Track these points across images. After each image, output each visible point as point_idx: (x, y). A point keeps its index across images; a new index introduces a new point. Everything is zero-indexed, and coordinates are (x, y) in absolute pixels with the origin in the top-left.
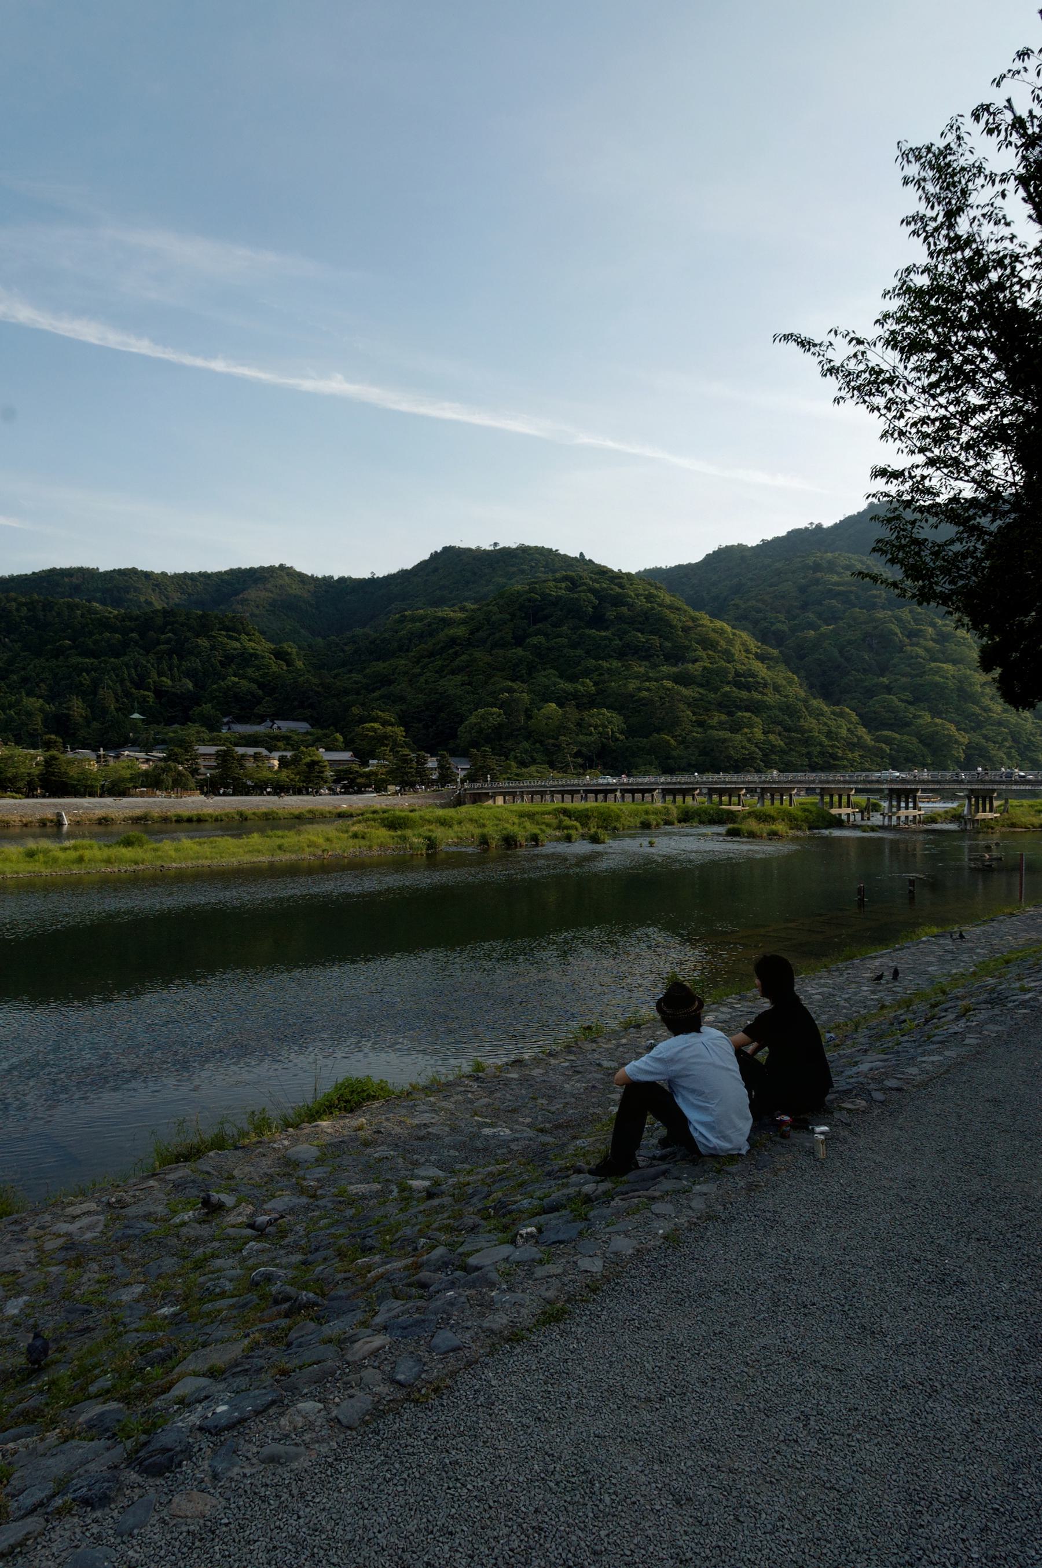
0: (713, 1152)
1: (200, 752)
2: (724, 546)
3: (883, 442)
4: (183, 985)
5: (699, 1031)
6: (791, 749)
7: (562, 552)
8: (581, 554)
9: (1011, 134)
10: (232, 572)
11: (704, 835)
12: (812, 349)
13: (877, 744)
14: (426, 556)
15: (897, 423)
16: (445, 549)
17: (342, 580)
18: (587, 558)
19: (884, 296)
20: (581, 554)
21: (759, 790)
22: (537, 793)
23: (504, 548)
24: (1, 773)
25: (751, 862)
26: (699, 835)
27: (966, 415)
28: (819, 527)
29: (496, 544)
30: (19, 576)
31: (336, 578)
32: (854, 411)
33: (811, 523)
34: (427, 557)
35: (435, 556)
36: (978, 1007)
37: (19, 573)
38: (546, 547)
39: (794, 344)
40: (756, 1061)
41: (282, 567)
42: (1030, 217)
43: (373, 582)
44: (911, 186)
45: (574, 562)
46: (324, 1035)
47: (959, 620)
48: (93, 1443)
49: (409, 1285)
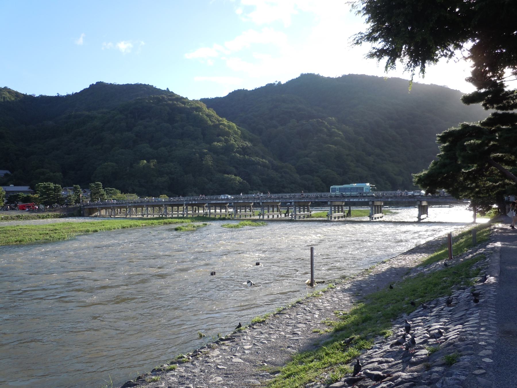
3: (358, 46)
4: (345, 317)
12: (356, 7)
14: (264, 85)
16: (97, 83)
18: (171, 90)
19: (58, 93)
20: (167, 88)
22: (175, 205)
24: (516, 74)
26: (121, 368)
30: (50, 96)
32: (426, 70)
33: (276, 81)
34: (88, 87)
35: (92, 86)
36: (115, 320)
37: (135, 83)
38: (150, 84)
39: (440, 58)
41: (5, 88)
42: (426, 73)
44: (415, 69)
45: (190, 101)
46: (360, 276)
48: (481, 379)
49: (455, 292)
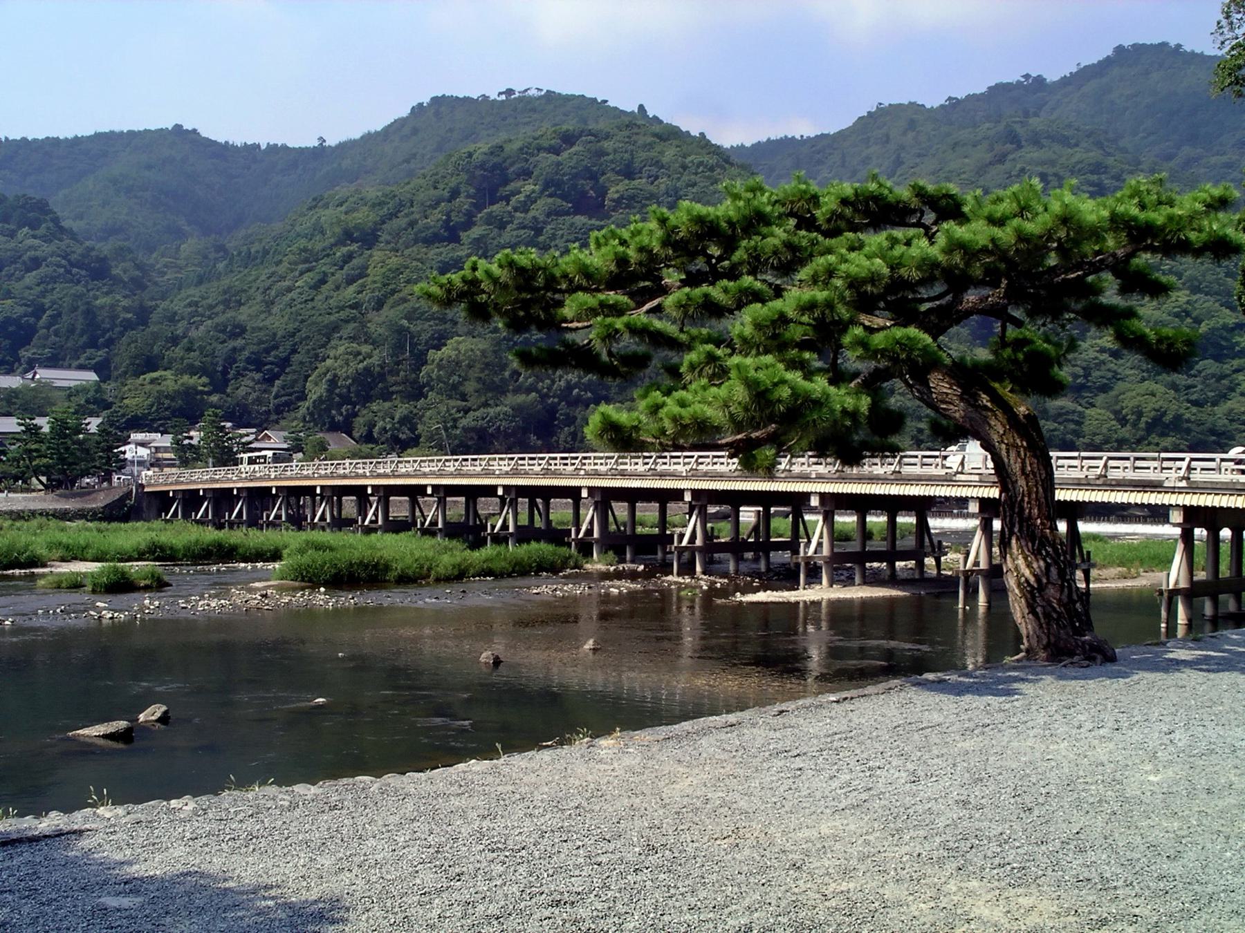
0: (88, 498)
1: (14, 420)
2: (373, 131)
5: (702, 134)
6: (1028, 475)
7: (611, 104)
8: (641, 107)
9: (1171, 231)
10: (98, 136)
11: (678, 738)
13: (698, 292)
15: (215, 344)
17: (273, 149)
18: (11, 138)
20: (641, 107)
21: (500, 492)
23: (1085, 67)
25: (956, 625)
27: (1017, 568)
28: (742, 145)
29: (1078, 64)
31: (263, 147)
40: (1226, 580)
43: (77, 141)
47: (323, 233)
